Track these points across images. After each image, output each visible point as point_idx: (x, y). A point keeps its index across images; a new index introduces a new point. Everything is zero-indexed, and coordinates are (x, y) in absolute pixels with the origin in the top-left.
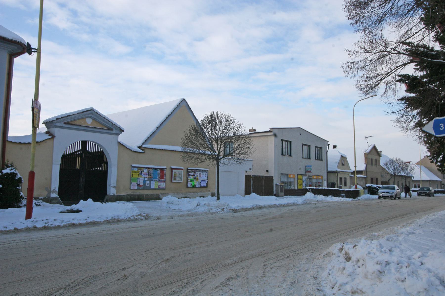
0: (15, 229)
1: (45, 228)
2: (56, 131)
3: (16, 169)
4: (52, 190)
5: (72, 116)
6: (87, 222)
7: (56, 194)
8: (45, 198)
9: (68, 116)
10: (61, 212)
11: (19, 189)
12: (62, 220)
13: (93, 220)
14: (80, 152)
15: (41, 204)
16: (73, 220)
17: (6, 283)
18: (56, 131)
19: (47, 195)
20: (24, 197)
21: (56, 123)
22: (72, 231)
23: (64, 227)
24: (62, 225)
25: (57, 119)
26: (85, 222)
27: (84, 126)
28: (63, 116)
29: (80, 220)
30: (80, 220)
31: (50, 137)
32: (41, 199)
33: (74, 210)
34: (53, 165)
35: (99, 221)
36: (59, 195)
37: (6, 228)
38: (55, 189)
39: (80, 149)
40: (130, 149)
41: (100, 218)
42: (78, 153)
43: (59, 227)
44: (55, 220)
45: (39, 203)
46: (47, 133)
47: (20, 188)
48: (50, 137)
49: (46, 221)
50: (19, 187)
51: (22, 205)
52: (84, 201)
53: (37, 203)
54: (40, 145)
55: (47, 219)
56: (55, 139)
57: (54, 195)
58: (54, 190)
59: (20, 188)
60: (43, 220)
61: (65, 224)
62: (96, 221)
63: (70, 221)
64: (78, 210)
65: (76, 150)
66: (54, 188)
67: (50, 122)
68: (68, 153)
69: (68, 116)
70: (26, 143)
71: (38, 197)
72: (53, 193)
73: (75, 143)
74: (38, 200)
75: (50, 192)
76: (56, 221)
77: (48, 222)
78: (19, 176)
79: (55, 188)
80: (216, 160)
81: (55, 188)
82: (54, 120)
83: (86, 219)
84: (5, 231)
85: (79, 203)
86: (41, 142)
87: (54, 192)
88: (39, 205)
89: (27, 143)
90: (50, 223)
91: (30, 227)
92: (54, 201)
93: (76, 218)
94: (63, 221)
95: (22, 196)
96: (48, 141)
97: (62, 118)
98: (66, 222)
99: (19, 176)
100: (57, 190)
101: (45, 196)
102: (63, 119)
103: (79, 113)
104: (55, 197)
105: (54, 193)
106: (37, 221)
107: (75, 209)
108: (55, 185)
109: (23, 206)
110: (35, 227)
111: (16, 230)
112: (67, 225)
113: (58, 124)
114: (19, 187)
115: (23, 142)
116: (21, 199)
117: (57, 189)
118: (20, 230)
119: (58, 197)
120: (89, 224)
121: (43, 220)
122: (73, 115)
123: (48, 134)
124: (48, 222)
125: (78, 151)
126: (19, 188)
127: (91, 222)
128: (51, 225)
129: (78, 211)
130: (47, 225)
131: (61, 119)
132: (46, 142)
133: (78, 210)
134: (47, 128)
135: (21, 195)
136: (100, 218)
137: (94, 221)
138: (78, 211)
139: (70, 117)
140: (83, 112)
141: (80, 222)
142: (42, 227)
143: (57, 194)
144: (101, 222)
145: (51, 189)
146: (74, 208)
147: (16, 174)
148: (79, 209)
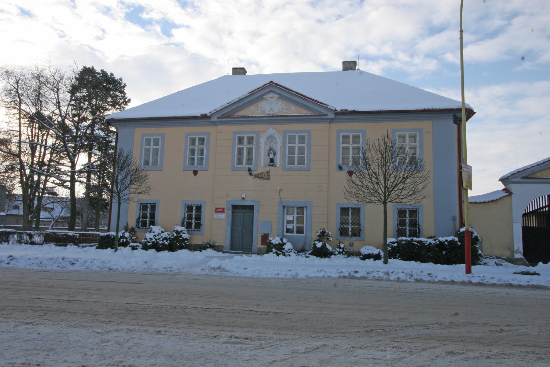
0: (452, 281)
1: (479, 284)
2: (514, 188)
3: (471, 228)
4: (515, 249)
5: (530, 169)
6: (529, 284)
7: (520, 254)
8: (508, 258)
9: (525, 170)
10: (515, 273)
11: (477, 248)
12: (500, 279)
13: (537, 283)
14: (547, 208)
15: (502, 263)
16: (512, 280)
17: (43, 272)
18: (514, 188)
19: (510, 255)
20: (482, 255)
21: (511, 179)
22: (451, 287)
23: (501, 285)
24: (499, 283)
25: (513, 175)
26: (526, 284)
27: (547, 178)
28: (519, 171)
29: (521, 281)
30: (521, 281)
31: (507, 194)
32: (503, 259)
33: (530, 272)
34: (514, 224)
35: (545, 285)
36: (524, 255)
37: (445, 279)
38: (518, 249)
39: (547, 204)
40: (491, 200)
41: (548, 282)
42: (544, 209)
43: (494, 285)
44: (492, 278)
45: (499, 263)
46: (504, 190)
47: (478, 246)
48: (507, 194)
49: (483, 278)
50: (477, 245)
51: (482, 263)
52: (544, 263)
53: (497, 263)
54: (496, 203)
55: (484, 276)
56: (513, 195)
57: (519, 256)
58: (517, 250)
59: (478, 246)
60: (479, 277)
61: (502, 283)
62: (540, 285)
63: (508, 281)
64: (535, 272)
65: (536, 208)
66: (518, 248)
67: (505, 179)
68: (531, 210)
69: (525, 169)
70: (478, 203)
71: (500, 256)
72: (516, 253)
73: (537, 199)
74: (500, 259)
75: (513, 252)
76: (493, 279)
77: (485, 279)
78: (476, 234)
79: (519, 248)
80: (383, 203)
81: (519, 248)
82: (509, 176)
83: (529, 282)
84: (443, 281)
85: (538, 266)
86: (497, 200)
87: (518, 252)
88: (501, 265)
89: (483, 202)
90: (486, 281)
91: (467, 281)
92: (519, 263)
93: (516, 279)
94: (501, 280)
95: (480, 254)
96: (504, 198)
97: (518, 172)
98: (504, 282)
99: (476, 234)
100: (522, 251)
101: (508, 256)
102: (519, 173)
103: (538, 165)
104: (519, 257)
105: (518, 253)
106: (473, 277)
107: (532, 272)
108: (519, 244)
109: (483, 264)
110: (470, 282)
111: (452, 282)
112: (504, 285)
113: (513, 180)
114: (477, 245)
115: (478, 201)
116: (480, 257)
117: (521, 250)
118: (456, 282)
119: (524, 258)
120: (530, 286)
121: (479, 277)
122: (531, 167)
123: (505, 192)
124: (485, 279)
125: (545, 207)
126: (476, 246)
127: (533, 285)
128: (487, 282)
129: (534, 274)
130: (482, 282)
131: (517, 174)
132: (503, 200)
133: (535, 272)
134: (504, 185)
135: (479, 253)
136: (548, 282)
137: (538, 284)
138: (534, 274)
139: (528, 170)
140: (544, 163)
141: (521, 283)
142: (477, 283)
143: (522, 254)
144: (548, 287)
145: (513, 248)
146: (530, 270)
147: (472, 233)
148: (536, 272)
